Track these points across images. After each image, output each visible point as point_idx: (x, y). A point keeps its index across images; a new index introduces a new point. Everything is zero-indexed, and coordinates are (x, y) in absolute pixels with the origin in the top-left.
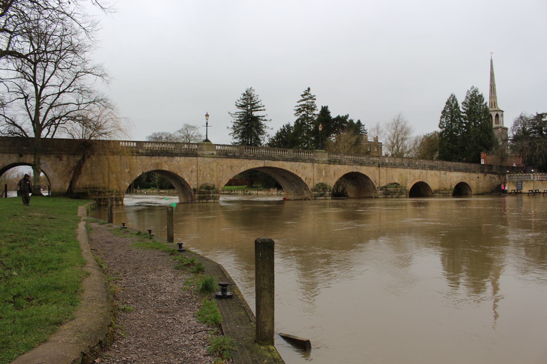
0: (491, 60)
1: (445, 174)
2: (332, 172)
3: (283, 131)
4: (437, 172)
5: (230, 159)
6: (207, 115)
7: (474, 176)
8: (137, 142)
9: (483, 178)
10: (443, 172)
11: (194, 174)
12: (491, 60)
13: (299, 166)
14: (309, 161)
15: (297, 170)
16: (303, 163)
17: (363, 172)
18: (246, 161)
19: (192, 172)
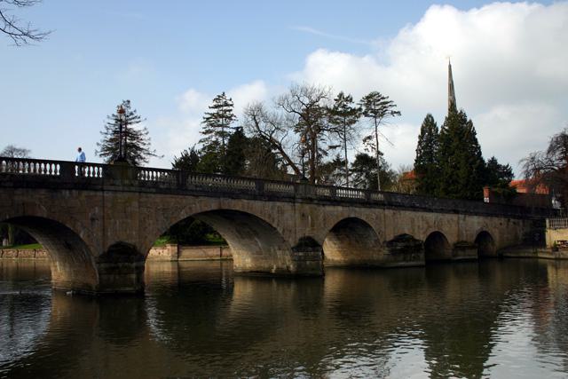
0: (450, 66)
1: (464, 220)
2: (321, 218)
3: (185, 158)
4: (455, 217)
5: (163, 196)
6: (80, 150)
7: (496, 220)
8: (61, 163)
9: (290, 208)
10: (462, 216)
11: (98, 223)
12: (450, 66)
13: (272, 208)
14: (287, 200)
15: (270, 215)
16: (278, 204)
17: (363, 218)
18: (190, 199)
19: (93, 220)
